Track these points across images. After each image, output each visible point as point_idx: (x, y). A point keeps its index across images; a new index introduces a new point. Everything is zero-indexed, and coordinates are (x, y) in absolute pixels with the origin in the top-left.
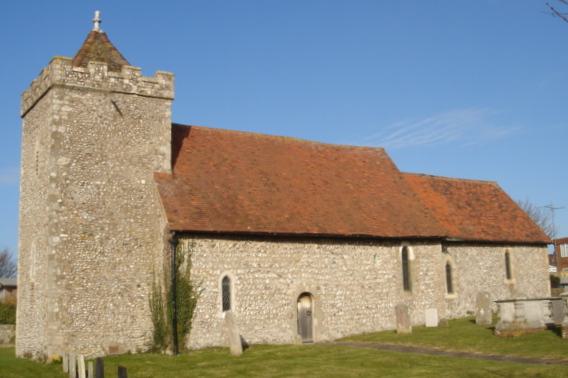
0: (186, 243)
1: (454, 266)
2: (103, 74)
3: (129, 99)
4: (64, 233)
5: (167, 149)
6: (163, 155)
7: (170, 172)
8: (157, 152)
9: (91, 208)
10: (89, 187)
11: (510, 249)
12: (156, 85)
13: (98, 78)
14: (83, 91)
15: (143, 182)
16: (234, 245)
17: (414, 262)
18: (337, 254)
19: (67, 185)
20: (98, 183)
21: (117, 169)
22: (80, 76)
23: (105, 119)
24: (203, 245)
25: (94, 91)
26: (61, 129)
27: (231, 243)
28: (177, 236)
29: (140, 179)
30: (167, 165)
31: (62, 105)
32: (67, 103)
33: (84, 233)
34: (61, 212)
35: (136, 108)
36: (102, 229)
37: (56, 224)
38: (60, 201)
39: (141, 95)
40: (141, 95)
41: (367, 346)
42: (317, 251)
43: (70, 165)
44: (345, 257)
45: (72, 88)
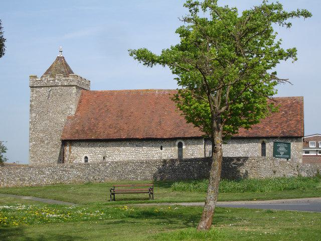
9: (43, 131)
11: (265, 140)
25: (44, 87)
28: (65, 142)
45: (36, 87)
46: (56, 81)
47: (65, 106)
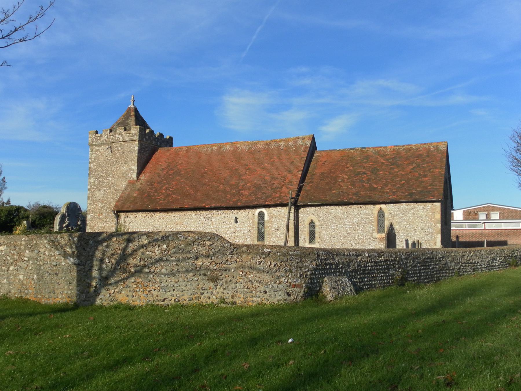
0: (122, 215)
1: (317, 223)
2: (108, 135)
3: (118, 145)
4: (92, 213)
5: (135, 168)
6: (133, 170)
7: (136, 179)
8: (131, 170)
9: (102, 201)
10: (101, 191)
11: (383, 206)
12: (130, 135)
13: (106, 137)
14: (100, 145)
15: (124, 186)
16: (146, 216)
17: (268, 221)
18: (208, 218)
19: (94, 191)
20: (105, 189)
21: (113, 181)
22: (98, 138)
23: (109, 157)
24: (131, 216)
25: (104, 144)
26: (92, 165)
27: (144, 215)
29: (122, 185)
30: (135, 176)
31: (92, 154)
32: (94, 152)
33: (99, 213)
34: (91, 204)
35: (122, 149)
36: (106, 210)
37: (89, 210)
38: (91, 199)
39: (124, 141)
40: (124, 141)
41: (497, 268)
42: (195, 217)
43: (94, 182)
44: (213, 220)
46: (117, 136)
47: (125, 168)
